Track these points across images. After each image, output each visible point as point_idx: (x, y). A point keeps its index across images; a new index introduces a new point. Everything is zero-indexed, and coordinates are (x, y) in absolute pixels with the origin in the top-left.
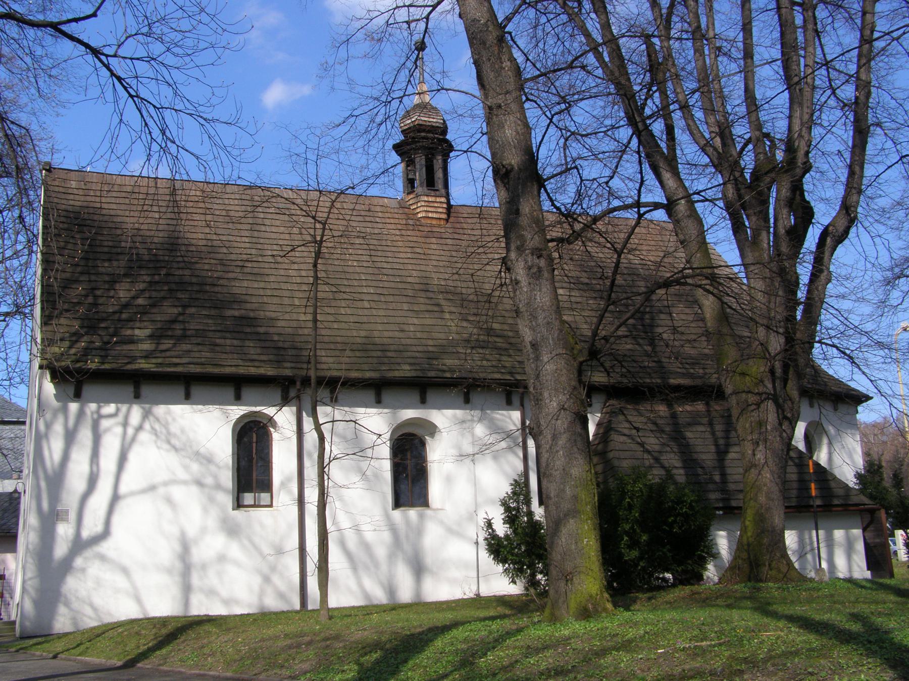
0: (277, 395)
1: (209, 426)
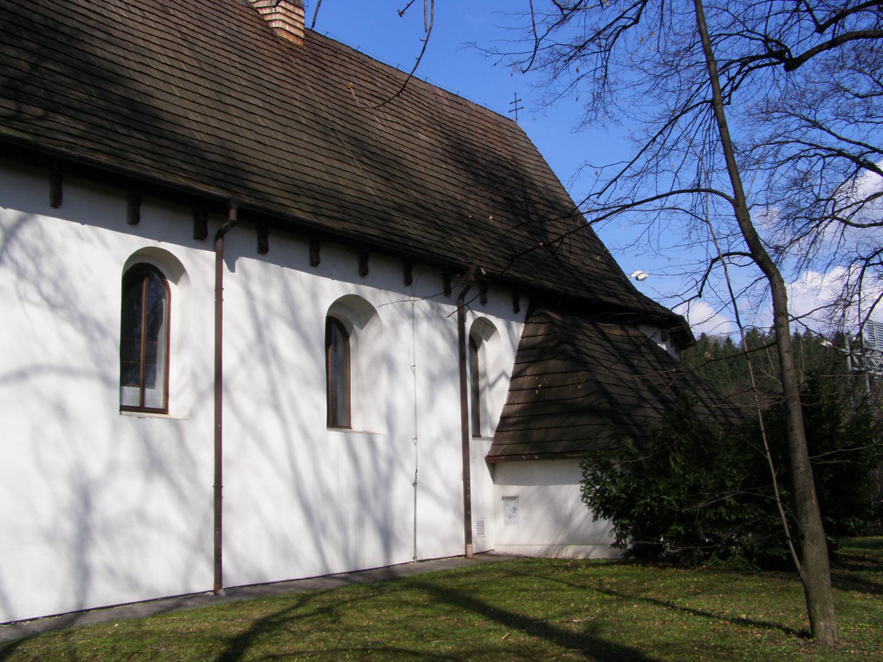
0: (188, 224)
1: (93, 254)
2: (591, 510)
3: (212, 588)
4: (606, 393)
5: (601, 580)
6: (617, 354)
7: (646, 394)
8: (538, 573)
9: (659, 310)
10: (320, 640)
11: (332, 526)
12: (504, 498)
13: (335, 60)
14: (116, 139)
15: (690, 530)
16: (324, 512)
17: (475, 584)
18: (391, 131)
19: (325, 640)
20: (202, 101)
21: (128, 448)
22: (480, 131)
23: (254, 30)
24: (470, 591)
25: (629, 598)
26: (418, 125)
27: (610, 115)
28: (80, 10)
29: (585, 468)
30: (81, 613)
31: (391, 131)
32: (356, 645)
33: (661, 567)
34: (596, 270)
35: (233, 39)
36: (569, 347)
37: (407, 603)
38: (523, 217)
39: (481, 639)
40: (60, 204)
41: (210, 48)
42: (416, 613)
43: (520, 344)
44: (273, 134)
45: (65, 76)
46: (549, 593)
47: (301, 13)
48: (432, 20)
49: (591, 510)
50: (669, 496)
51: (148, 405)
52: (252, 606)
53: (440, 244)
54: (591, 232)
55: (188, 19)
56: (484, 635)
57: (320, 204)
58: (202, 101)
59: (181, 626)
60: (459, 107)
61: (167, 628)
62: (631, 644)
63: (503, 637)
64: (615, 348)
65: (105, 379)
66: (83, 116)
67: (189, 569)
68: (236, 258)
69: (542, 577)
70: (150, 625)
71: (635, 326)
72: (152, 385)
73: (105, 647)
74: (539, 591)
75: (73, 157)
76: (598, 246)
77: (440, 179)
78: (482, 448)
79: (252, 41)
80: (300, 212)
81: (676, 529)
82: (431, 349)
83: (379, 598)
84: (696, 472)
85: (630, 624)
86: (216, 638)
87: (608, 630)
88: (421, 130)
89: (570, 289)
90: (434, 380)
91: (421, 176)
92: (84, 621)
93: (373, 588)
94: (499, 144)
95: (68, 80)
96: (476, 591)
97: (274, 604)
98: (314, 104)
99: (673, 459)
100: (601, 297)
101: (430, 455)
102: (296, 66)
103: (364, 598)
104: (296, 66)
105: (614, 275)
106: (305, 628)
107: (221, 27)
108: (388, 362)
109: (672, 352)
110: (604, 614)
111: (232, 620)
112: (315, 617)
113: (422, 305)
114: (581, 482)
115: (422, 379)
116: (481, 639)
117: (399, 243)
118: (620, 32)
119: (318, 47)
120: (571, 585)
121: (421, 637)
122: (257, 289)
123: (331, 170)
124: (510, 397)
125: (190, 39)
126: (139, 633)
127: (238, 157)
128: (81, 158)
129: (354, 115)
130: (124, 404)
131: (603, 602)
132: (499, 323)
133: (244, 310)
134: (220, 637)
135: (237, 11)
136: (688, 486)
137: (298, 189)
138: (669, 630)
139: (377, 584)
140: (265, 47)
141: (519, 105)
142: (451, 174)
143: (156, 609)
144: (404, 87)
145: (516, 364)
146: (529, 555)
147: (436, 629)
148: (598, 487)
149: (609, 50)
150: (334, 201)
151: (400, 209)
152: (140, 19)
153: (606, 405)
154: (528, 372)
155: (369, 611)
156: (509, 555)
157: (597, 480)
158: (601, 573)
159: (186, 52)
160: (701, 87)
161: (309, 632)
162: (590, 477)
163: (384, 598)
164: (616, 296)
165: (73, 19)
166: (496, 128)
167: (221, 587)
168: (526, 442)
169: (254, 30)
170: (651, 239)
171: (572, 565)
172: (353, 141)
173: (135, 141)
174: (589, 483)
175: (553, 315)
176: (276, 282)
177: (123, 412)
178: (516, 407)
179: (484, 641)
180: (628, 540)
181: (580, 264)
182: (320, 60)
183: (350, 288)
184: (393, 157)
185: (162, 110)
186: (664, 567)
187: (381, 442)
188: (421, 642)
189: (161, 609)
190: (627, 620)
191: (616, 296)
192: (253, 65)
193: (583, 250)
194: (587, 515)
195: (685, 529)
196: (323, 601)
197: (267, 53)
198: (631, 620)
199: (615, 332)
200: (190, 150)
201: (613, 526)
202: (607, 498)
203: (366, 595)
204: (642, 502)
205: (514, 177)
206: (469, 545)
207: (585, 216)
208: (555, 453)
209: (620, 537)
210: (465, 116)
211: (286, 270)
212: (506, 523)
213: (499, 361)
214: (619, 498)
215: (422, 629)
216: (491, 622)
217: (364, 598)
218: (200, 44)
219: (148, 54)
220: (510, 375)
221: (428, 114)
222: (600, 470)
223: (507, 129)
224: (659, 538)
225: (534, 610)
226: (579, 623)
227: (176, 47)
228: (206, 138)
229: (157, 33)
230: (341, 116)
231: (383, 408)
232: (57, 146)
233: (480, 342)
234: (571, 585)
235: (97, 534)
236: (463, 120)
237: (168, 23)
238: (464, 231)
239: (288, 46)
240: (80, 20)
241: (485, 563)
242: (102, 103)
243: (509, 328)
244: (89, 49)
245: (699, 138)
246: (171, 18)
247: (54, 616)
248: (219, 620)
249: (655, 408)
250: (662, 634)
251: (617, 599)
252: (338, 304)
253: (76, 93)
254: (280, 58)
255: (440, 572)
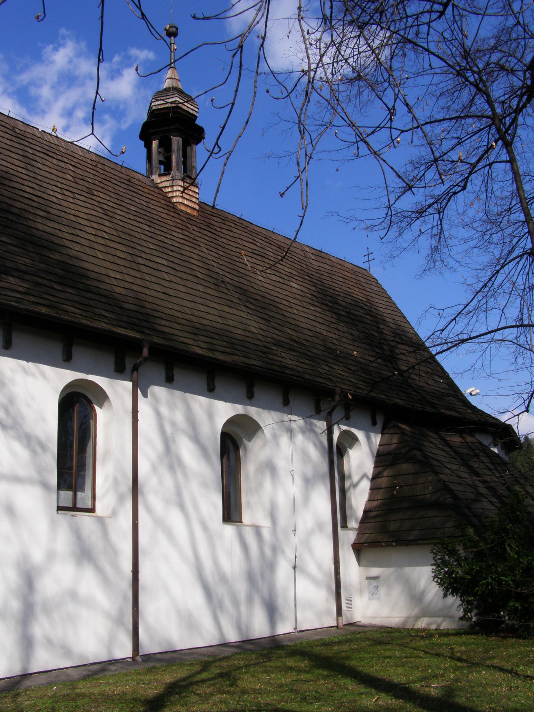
1: (36, 387)
2: (441, 588)
3: (131, 655)
4: (450, 491)
5: (452, 649)
6: (457, 458)
7: (482, 489)
8: (399, 642)
9: (491, 420)
10: (221, 702)
11: (227, 603)
12: (368, 578)
13: (223, 226)
14: (54, 294)
15: (526, 605)
16: (220, 591)
17: (346, 651)
18: (269, 282)
19: (225, 702)
20: (119, 262)
21: (63, 541)
22: (340, 279)
23: (159, 205)
24: (343, 658)
25: (477, 665)
26: (291, 276)
27: (445, 263)
28: (26, 195)
29: (435, 554)
30: (25, 676)
31: (269, 282)
32: (251, 706)
33: (502, 637)
34: (438, 389)
35: (143, 212)
36: (418, 453)
37: (291, 669)
38: (377, 347)
39: (355, 701)
40: (10, 346)
41: (125, 220)
42: (299, 677)
43: (378, 451)
44: (176, 286)
45: (15, 246)
46: (410, 660)
47: (196, 190)
48: (307, 200)
49: (441, 588)
50: (506, 577)
51: (79, 505)
52: (164, 671)
53: (311, 372)
54: (436, 361)
55: (108, 198)
56: (358, 698)
57: (215, 342)
58: (119, 262)
59: (107, 689)
60: (322, 260)
61: (96, 691)
62: (484, 708)
63: (373, 699)
64: (456, 452)
65: (45, 485)
66: (27, 277)
67: (112, 640)
68: (148, 387)
69: (403, 646)
70: (82, 688)
71: (471, 432)
72: (82, 490)
73: (46, 708)
74: (401, 658)
75: (19, 308)
76: (439, 369)
77: (309, 319)
78: (348, 537)
79: (158, 213)
80: (198, 349)
81: (514, 605)
82: (305, 456)
83: (268, 664)
84: (527, 556)
85: (480, 689)
86: (136, 700)
87: (462, 694)
88: (293, 280)
89: (417, 405)
90: (308, 482)
91: (294, 317)
92: (28, 683)
93: (262, 655)
94: (356, 289)
95: (17, 249)
96: (348, 658)
97: (182, 670)
98: (208, 262)
99: (509, 545)
100: (442, 411)
101: (307, 544)
102: (193, 232)
103: (256, 664)
104: (193, 232)
105: (453, 393)
106: (209, 690)
107: (134, 203)
108: (270, 467)
109: (502, 455)
110: (457, 680)
111: (148, 684)
112: (217, 681)
113: (297, 421)
114: (432, 565)
115: (298, 481)
116: (355, 701)
117: (278, 371)
118: (451, 197)
119: (209, 217)
120: (427, 653)
121: (304, 699)
122: (164, 410)
123: (223, 314)
124: (371, 495)
125: (110, 214)
126: (73, 695)
127: (148, 306)
128: (26, 310)
129: (240, 270)
130: (60, 505)
131: (456, 668)
132: (360, 434)
133: (154, 428)
134: (140, 699)
135: (146, 191)
136: (522, 568)
137: (196, 330)
138: (516, 696)
139: (265, 652)
140: (168, 217)
141: (371, 257)
142: (318, 315)
143: (85, 673)
144: (285, 250)
145: (375, 467)
146: (390, 626)
147: (317, 692)
148: (446, 569)
149: (443, 212)
150: (225, 339)
151: (278, 344)
152: (71, 200)
153: (449, 500)
154: (385, 474)
155: (260, 675)
156: (373, 626)
157: (445, 564)
158: (452, 642)
159: (107, 224)
160: (519, 240)
161: (212, 694)
162: (439, 561)
163: (272, 664)
164: (454, 410)
165: (21, 202)
166: (353, 276)
167: (138, 654)
168: (384, 532)
169: (159, 205)
170: (484, 365)
171: (426, 634)
172: (238, 290)
173: (68, 295)
174: (439, 565)
175: (404, 427)
176: (180, 404)
177: (60, 512)
178: (375, 503)
179: (358, 703)
180: (473, 614)
181: (425, 385)
182: (211, 226)
183: (238, 409)
184: (271, 303)
185: (89, 270)
186: (505, 637)
187: (266, 533)
188: (305, 704)
189: (90, 673)
190: (478, 685)
191: (454, 410)
192: (159, 232)
193: (426, 373)
194: (437, 592)
195: (522, 606)
196: (222, 667)
197: (170, 222)
198: (481, 686)
199: (455, 439)
200: (111, 301)
201: (461, 602)
202: (454, 578)
203: (257, 661)
204: (484, 581)
205: (369, 315)
206: (340, 618)
207: (431, 349)
208: (410, 541)
209: (466, 611)
210: (327, 267)
211: (188, 395)
212: (370, 599)
213: (361, 465)
214: (464, 578)
215: (306, 692)
216: (363, 686)
217: (256, 664)
218: (118, 217)
219: (78, 226)
220: (371, 477)
221: (299, 267)
222: (447, 555)
223: (362, 277)
224: (500, 612)
225: (397, 675)
226: (437, 687)
227: (99, 221)
228: (123, 291)
229: (85, 210)
230: (230, 271)
231: (268, 506)
232: (9, 301)
233: (346, 450)
234: (427, 653)
235: (38, 610)
236: (327, 271)
237: (93, 202)
238: (330, 360)
239: (187, 216)
240: (26, 202)
241: (353, 633)
242: (42, 266)
243: (368, 438)
244: (31, 224)
245: (520, 281)
246: (95, 198)
247: (4, 679)
248: (138, 683)
249: (491, 502)
250: (510, 700)
251: (468, 666)
252: (230, 422)
253: (22, 259)
254: (180, 226)
255: (317, 641)
